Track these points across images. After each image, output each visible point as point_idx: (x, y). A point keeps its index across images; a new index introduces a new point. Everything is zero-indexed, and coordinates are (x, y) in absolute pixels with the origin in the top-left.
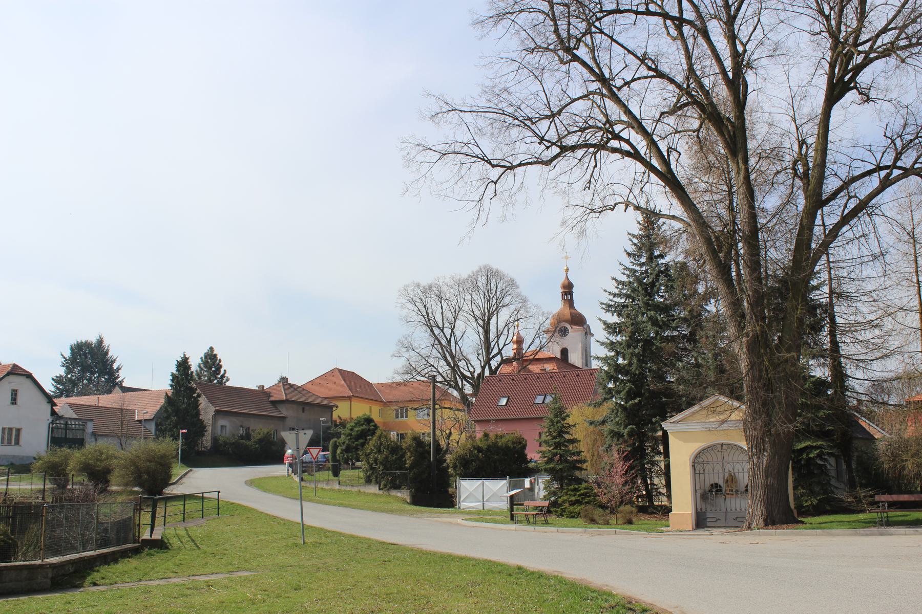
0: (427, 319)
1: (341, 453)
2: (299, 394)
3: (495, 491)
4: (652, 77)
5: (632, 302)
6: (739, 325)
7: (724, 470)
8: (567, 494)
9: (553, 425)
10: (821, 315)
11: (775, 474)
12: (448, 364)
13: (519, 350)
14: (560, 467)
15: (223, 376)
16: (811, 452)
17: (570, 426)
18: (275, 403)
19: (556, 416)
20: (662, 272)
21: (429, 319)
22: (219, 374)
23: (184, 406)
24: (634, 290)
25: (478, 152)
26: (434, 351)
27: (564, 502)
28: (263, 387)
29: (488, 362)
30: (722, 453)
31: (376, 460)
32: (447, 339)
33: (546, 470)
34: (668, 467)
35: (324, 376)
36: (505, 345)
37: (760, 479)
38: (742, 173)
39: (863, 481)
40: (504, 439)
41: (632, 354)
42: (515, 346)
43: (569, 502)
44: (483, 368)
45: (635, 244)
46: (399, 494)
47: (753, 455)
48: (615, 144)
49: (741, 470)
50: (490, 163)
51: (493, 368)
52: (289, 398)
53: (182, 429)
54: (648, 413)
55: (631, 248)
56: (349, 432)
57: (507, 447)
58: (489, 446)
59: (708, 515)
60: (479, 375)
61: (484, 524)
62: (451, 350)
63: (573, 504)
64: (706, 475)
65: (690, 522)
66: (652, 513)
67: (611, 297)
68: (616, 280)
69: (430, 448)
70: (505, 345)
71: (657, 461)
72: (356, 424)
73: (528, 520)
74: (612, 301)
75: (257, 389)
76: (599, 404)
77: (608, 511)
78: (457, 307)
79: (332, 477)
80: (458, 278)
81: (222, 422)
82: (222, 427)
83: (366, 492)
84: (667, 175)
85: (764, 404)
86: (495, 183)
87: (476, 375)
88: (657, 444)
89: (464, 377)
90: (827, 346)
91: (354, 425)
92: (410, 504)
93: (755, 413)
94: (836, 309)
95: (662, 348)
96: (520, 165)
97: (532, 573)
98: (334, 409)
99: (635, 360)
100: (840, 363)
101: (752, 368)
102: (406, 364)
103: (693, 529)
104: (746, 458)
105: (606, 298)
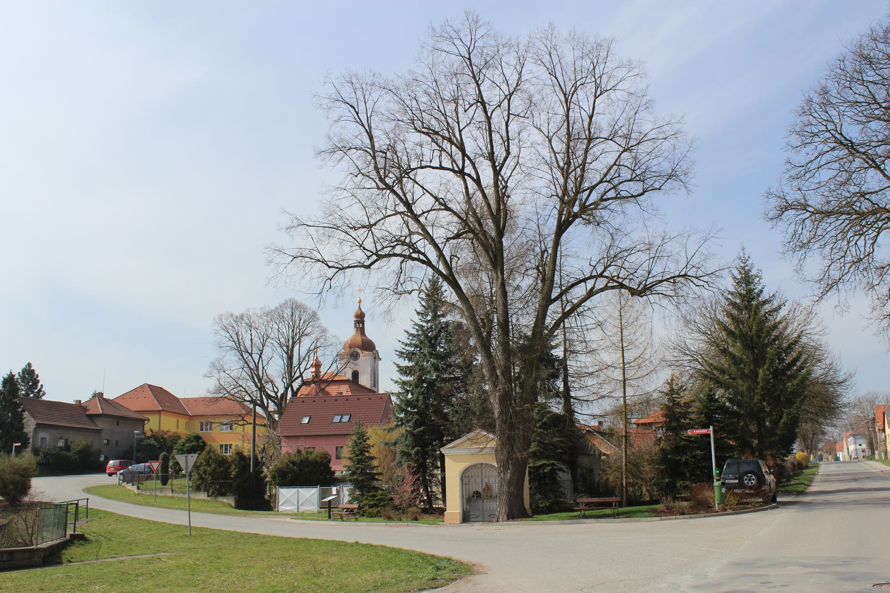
0: (238, 345)
1: (173, 465)
2: (113, 408)
3: (308, 497)
4: (442, 209)
5: (419, 351)
6: (494, 384)
7: (482, 481)
8: (367, 499)
9: (357, 445)
10: (558, 366)
11: (516, 485)
12: (256, 386)
13: (317, 372)
14: (362, 478)
15: (40, 391)
16: (546, 468)
17: (369, 447)
18: (92, 417)
19: (359, 439)
20: (443, 328)
21: (240, 345)
22: (36, 388)
23: (9, 420)
24: (421, 342)
25: (319, 257)
26: (244, 374)
27: (365, 505)
28: (80, 401)
29: (290, 385)
30: (482, 470)
31: (205, 472)
32: (255, 363)
33: (351, 481)
34: (444, 479)
35: (134, 391)
36: (305, 369)
37: (505, 488)
38: (500, 280)
39: (583, 489)
40: (313, 455)
41: (419, 393)
42: (314, 370)
43: (369, 505)
44: (287, 389)
45: (423, 306)
46: (225, 500)
47: (501, 472)
48: (415, 255)
49: (494, 482)
50: (327, 265)
51: (295, 389)
52: (105, 412)
53: (16, 443)
54: (430, 437)
55: (420, 309)
56: (180, 447)
57: (316, 462)
58: (302, 461)
59: (471, 513)
60: (282, 395)
61: (309, 522)
62: (258, 374)
63: (371, 506)
64: (471, 486)
65: (459, 518)
66: (432, 513)
67: (404, 346)
68: (407, 332)
69: (250, 461)
70: (305, 369)
71: (436, 474)
72: (187, 440)
73: (342, 518)
74: (404, 349)
75: (74, 403)
76: (391, 430)
77: (401, 511)
78: (265, 336)
79: (161, 486)
80: (267, 309)
81: (42, 434)
82: (42, 438)
83: (196, 498)
84: (449, 276)
85: (509, 438)
86: (331, 280)
87: (279, 395)
88: (435, 460)
89: (269, 397)
90: (562, 389)
91: (185, 441)
92: (235, 508)
93: (503, 444)
94: (568, 363)
95: (441, 388)
96: (349, 267)
97: (365, 545)
98: (146, 422)
99: (421, 398)
100: (570, 402)
101: (502, 413)
102: (217, 383)
103: (461, 523)
104: (497, 474)
105: (400, 347)
